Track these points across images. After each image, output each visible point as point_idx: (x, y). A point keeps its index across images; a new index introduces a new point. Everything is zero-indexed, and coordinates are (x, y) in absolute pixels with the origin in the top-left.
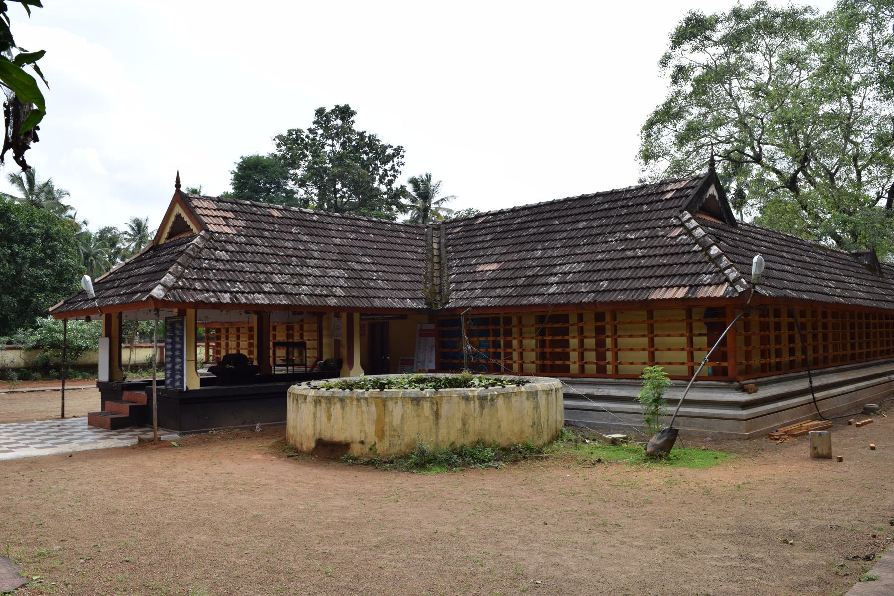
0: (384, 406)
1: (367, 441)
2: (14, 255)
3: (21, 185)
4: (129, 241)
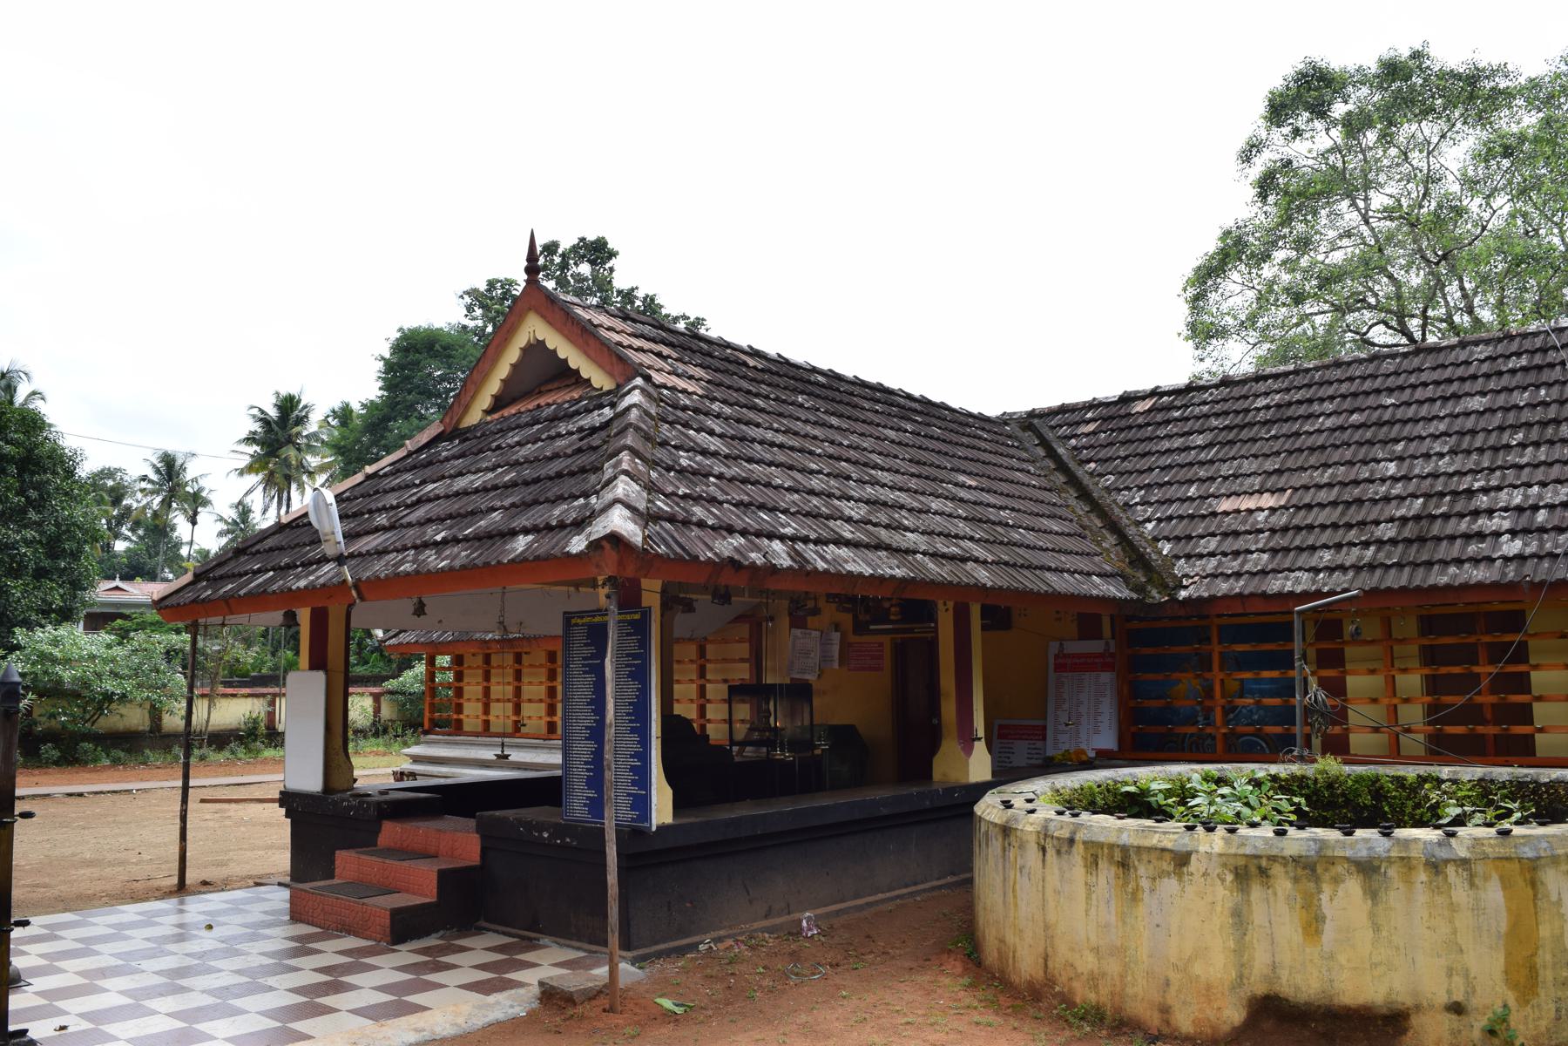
0: (1533, 884)
1: (1475, 1002)
4: (152, 492)
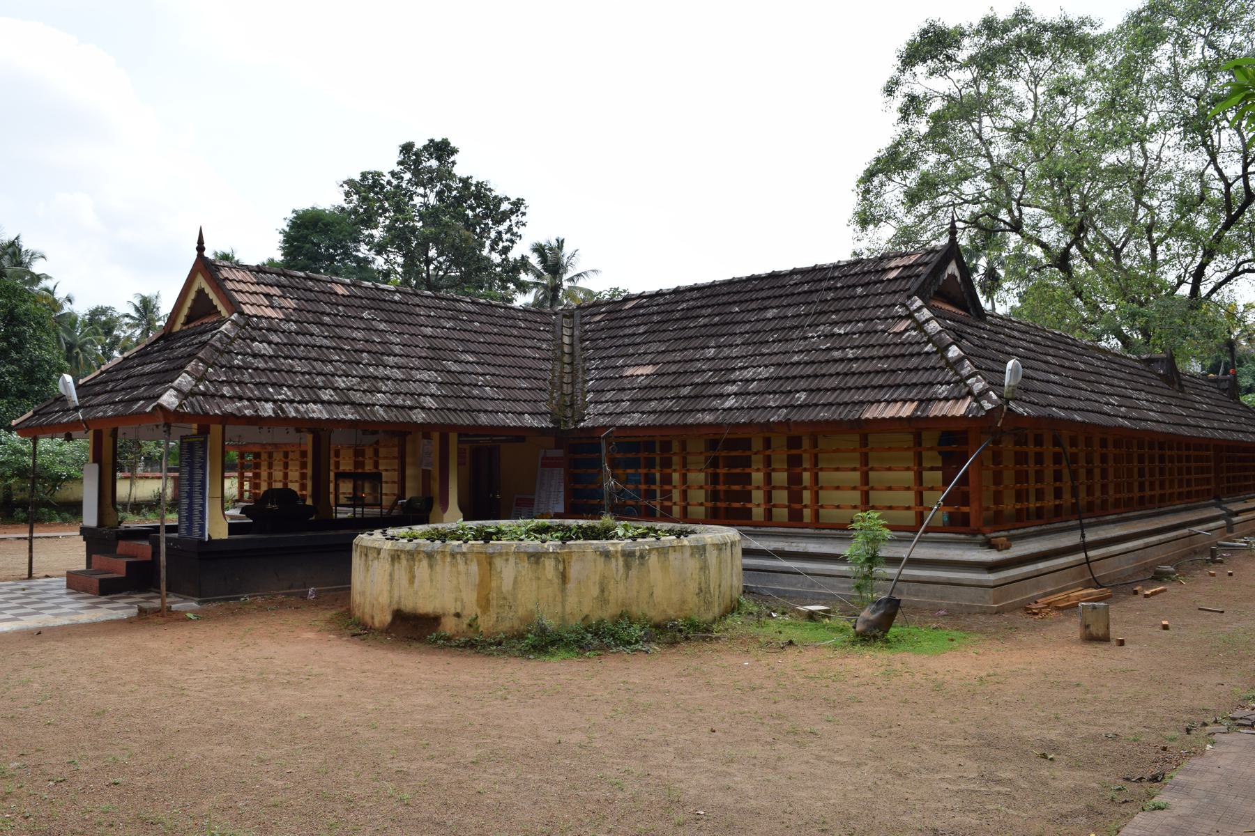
1: (465, 613)
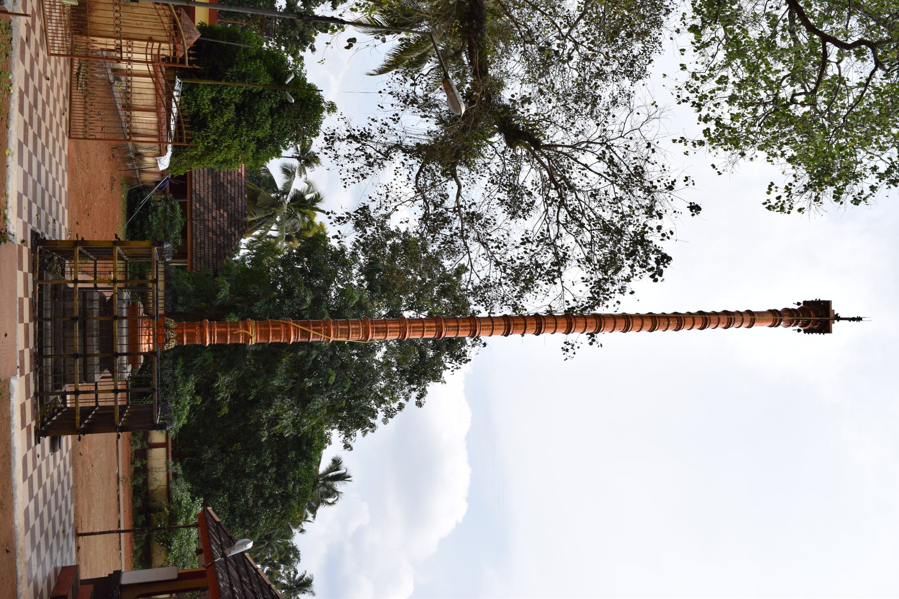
2: (265, 469)
3: (331, 469)
4: (289, 578)
